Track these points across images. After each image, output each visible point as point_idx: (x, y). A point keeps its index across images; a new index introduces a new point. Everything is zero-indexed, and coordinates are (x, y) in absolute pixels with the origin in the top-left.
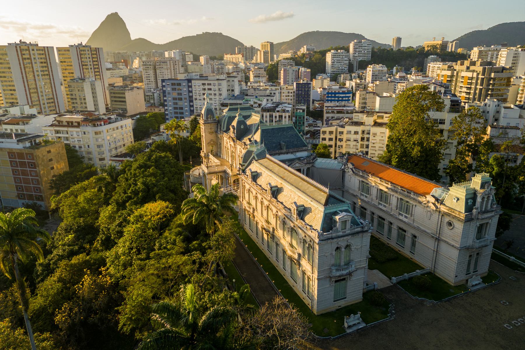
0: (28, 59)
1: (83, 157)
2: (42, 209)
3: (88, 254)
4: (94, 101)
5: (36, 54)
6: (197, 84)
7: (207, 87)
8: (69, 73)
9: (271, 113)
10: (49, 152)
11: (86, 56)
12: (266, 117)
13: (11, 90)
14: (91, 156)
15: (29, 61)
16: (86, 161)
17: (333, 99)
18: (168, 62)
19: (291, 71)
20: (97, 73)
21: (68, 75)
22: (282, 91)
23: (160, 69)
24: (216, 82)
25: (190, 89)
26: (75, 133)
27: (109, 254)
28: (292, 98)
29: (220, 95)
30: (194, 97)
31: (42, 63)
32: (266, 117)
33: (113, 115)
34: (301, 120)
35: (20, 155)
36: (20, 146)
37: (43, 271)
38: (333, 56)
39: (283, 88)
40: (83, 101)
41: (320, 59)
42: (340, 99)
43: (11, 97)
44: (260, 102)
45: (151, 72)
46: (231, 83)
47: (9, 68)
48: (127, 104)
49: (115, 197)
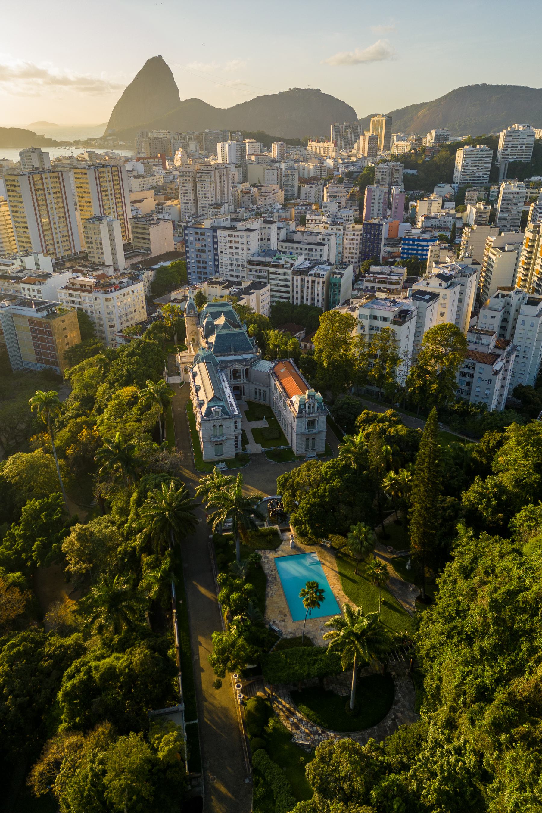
0: (41, 189)
1: (95, 323)
2: (57, 373)
3: (88, 417)
4: (111, 244)
5: (50, 183)
6: (222, 235)
7: (233, 239)
8: (86, 202)
9: (303, 276)
10: (63, 321)
11: (105, 179)
12: (297, 281)
13: (23, 227)
14: (102, 322)
15: (42, 192)
16: (97, 327)
17: (410, 247)
18: (212, 173)
19: (377, 193)
20: (119, 200)
21: (85, 204)
22: (346, 233)
23: (202, 183)
24: (244, 234)
25: (215, 240)
26: (87, 298)
27: (99, 418)
28: (357, 242)
29: (249, 249)
30: (219, 250)
31: (56, 193)
32: (297, 281)
33: (125, 278)
34: (336, 288)
35: (39, 323)
36: (39, 315)
37: (59, 425)
38: (467, 156)
39: (348, 228)
40: (99, 246)
41: (447, 159)
42: (420, 248)
43: (23, 235)
44: (292, 262)
45: (190, 186)
46: (266, 231)
47: (22, 202)
48: (152, 242)
49: (109, 378)
